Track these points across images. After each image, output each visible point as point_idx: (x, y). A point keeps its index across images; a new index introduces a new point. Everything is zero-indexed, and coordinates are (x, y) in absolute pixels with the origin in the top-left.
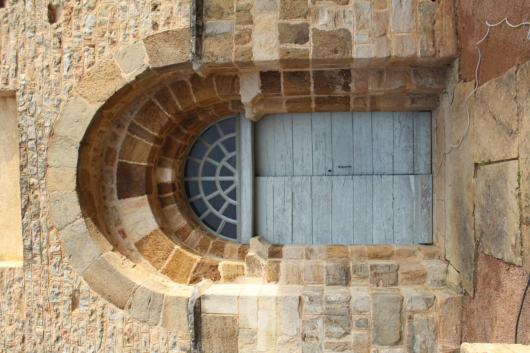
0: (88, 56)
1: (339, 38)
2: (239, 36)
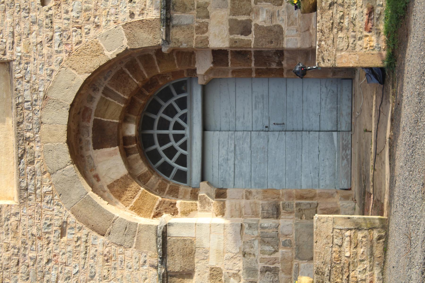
0: (76, 36)
1: (274, 32)
2: (198, 28)
